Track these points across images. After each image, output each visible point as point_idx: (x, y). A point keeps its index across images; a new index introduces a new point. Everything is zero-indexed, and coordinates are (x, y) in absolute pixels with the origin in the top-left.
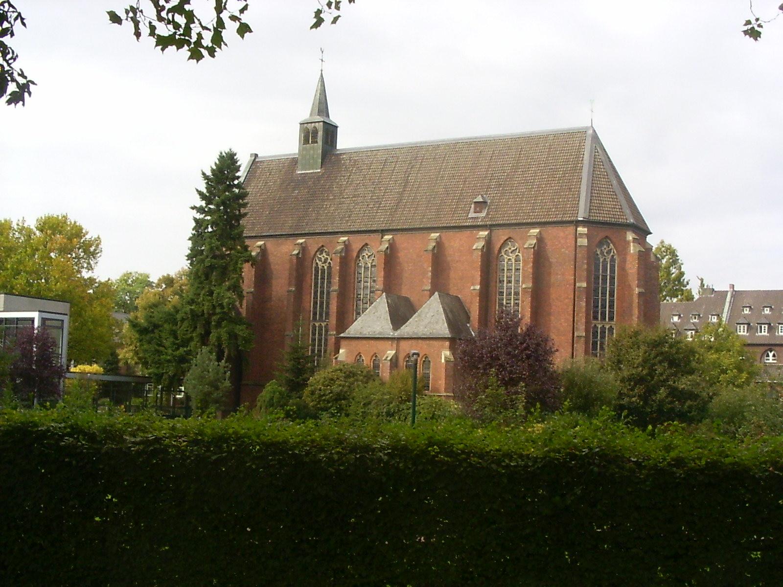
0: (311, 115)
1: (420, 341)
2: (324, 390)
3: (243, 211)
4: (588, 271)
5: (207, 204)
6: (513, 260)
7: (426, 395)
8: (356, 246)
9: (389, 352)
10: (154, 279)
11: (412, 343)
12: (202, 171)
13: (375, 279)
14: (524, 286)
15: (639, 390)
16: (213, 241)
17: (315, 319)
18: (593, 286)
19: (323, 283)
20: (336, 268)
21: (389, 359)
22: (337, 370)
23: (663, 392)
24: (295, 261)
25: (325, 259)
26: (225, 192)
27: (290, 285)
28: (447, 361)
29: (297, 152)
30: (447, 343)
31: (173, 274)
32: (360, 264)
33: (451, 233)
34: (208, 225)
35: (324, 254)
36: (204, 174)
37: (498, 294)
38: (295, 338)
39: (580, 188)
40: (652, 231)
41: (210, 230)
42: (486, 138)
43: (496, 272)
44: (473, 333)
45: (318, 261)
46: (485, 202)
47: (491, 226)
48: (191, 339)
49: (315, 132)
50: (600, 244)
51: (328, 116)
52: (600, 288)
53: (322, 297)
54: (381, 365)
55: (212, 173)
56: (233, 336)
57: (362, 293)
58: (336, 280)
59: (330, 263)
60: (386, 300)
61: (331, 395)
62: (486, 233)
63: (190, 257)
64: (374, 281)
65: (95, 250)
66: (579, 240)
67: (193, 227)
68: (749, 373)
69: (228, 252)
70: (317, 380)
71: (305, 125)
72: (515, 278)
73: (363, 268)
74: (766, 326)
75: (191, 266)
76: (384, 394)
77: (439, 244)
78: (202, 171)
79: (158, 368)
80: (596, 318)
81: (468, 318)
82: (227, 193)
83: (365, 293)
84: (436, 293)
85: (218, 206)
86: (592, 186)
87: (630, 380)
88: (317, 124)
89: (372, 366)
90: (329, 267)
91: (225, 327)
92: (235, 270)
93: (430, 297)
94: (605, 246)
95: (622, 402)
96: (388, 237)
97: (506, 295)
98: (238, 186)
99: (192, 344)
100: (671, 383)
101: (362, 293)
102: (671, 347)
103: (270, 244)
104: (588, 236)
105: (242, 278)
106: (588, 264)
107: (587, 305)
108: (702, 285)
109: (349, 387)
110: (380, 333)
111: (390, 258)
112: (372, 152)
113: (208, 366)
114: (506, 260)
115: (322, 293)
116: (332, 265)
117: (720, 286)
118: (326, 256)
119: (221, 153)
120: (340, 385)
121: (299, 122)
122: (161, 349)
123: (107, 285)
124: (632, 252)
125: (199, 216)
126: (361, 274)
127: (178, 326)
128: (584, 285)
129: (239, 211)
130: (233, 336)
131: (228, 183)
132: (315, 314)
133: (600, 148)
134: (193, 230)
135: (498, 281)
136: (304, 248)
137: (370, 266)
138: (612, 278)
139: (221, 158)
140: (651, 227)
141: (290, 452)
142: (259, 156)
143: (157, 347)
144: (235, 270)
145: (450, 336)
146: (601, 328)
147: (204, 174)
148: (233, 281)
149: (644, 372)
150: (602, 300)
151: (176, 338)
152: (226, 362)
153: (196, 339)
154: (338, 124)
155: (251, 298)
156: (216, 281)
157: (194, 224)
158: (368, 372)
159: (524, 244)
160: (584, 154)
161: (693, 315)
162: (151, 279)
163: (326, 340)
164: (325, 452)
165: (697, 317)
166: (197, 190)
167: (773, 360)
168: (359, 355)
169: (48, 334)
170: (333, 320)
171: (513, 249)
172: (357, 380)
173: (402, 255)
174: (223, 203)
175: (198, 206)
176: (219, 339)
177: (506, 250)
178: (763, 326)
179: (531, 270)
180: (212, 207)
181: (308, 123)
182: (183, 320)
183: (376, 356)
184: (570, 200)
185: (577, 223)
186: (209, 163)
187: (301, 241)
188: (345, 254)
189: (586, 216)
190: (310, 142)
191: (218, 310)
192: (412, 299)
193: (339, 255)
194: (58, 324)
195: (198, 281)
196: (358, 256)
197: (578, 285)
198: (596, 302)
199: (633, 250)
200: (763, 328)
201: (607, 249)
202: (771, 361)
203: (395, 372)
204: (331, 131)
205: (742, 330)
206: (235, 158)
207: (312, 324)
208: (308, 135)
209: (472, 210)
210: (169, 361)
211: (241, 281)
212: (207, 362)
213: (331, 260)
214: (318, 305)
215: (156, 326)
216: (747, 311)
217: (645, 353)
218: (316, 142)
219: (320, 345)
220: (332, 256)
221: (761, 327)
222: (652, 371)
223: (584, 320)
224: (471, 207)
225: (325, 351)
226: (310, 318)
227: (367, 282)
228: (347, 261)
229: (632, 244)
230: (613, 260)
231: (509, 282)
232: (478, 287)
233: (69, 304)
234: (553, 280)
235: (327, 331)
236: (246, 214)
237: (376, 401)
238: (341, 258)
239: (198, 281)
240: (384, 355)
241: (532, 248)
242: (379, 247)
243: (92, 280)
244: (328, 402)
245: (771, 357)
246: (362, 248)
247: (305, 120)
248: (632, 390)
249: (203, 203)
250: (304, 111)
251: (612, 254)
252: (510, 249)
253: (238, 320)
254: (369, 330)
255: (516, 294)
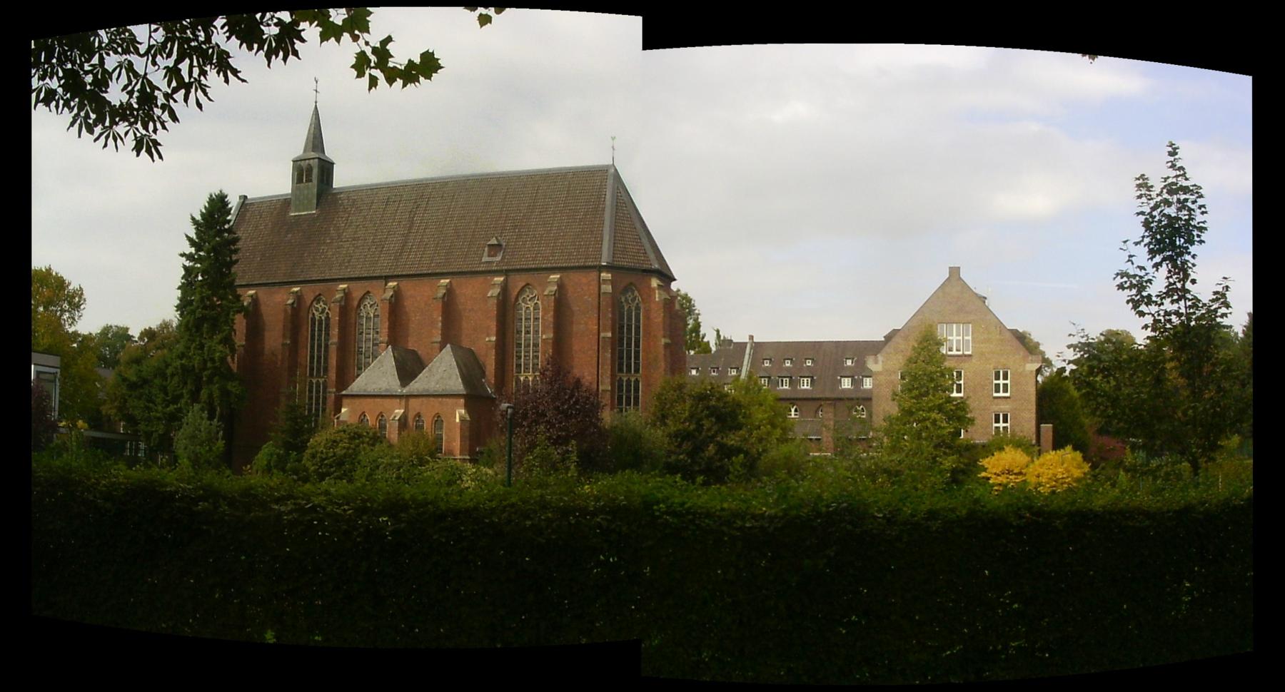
0: (305, 151)
1: (432, 399)
2: (327, 453)
3: (234, 257)
4: (613, 320)
5: (197, 251)
6: (532, 309)
7: (440, 459)
8: (357, 294)
9: (397, 411)
10: (135, 332)
12: (191, 216)
13: (379, 330)
14: (544, 337)
15: (687, 446)
16: (204, 290)
17: (311, 375)
18: (617, 335)
19: (320, 336)
20: (335, 319)
21: (397, 418)
22: (339, 431)
23: (712, 449)
24: (290, 311)
25: (322, 310)
26: (215, 237)
27: (284, 336)
28: (462, 420)
29: (290, 192)
30: (462, 401)
31: (154, 326)
32: (362, 314)
33: (462, 280)
34: (198, 273)
35: (321, 303)
36: (193, 219)
37: (515, 346)
38: (291, 396)
39: (602, 230)
40: (676, 277)
41: (200, 278)
42: (499, 174)
43: (514, 323)
44: (489, 389)
45: (314, 312)
46: (499, 245)
47: (507, 271)
48: (181, 396)
49: (310, 169)
50: (626, 290)
51: (323, 151)
52: (625, 339)
53: (319, 351)
54: (388, 425)
55: (201, 216)
56: (225, 393)
57: (364, 346)
58: (335, 331)
59: (327, 313)
60: (392, 354)
61: (335, 458)
62: (502, 279)
63: (179, 308)
64: (377, 333)
65: (79, 301)
66: (603, 287)
67: (181, 276)
68: (782, 429)
69: (219, 302)
70: (318, 441)
71: (299, 162)
72: (534, 328)
73: (365, 319)
74: (788, 379)
75: (181, 317)
76: (393, 457)
77: (450, 291)
78: (191, 216)
79: (147, 425)
80: (621, 370)
81: (483, 374)
82: (218, 239)
83: (367, 346)
84: (448, 346)
85: (208, 252)
86: (615, 229)
87: (676, 436)
88: (312, 161)
89: (378, 426)
90: (328, 318)
91: (217, 383)
92: (226, 322)
93: (441, 351)
95: (669, 460)
96: (392, 284)
97: (525, 347)
98: (230, 231)
99: (183, 401)
100: (719, 439)
101: (364, 346)
102: (718, 400)
103: (263, 293)
104: (613, 282)
105: (235, 331)
106: (613, 313)
107: (612, 357)
108: (718, 336)
109: (354, 449)
110: (387, 390)
111: (396, 308)
112: (373, 190)
113: (199, 425)
114: (524, 309)
115: (319, 346)
116: (330, 316)
117: (739, 337)
118: (323, 306)
119: (211, 196)
120: (344, 448)
121: (292, 159)
122: (151, 405)
123: (87, 338)
124: (657, 299)
125: (188, 264)
126: (362, 325)
127: (169, 382)
128: (609, 335)
129: (231, 257)
130: (225, 393)
131: (218, 228)
132: (312, 369)
133: (623, 188)
134: (182, 278)
135: (515, 331)
136: (299, 297)
137: (372, 315)
138: (638, 328)
139: (211, 200)
140: (675, 271)
141: (487, 521)
142: (248, 197)
143: (146, 404)
144: (226, 322)
145: (465, 393)
147: (193, 219)
148: (224, 334)
149: (692, 427)
150: (627, 351)
151: (166, 394)
152: (218, 421)
153: (186, 396)
154: (335, 162)
155: (243, 352)
156: (207, 333)
157: (183, 273)
158: (375, 433)
159: (543, 291)
160: (605, 195)
161: (712, 368)
162: (130, 333)
163: (325, 398)
164: (531, 519)
165: (716, 370)
166: (187, 236)
167: (795, 415)
168: (363, 414)
169: (42, 387)
170: (333, 375)
171: (531, 296)
172: (363, 443)
173: (408, 304)
174: (214, 249)
175: (187, 253)
176: (210, 396)
177: (524, 298)
178: (784, 379)
179: (551, 320)
180: (202, 253)
181: (301, 160)
182: (173, 375)
183: (382, 416)
184: (593, 243)
185: (601, 269)
186: (198, 206)
187: (296, 289)
188: (345, 303)
189: (610, 260)
191: (209, 365)
192: (420, 352)
193: (338, 304)
194: (51, 377)
195: (188, 333)
196: (359, 306)
197: (602, 335)
198: (621, 352)
199: (659, 298)
200: (784, 382)
201: (632, 296)
202: (793, 416)
203: (404, 434)
204: (326, 168)
205: (805, 384)
206: (226, 200)
207: (308, 380)
208: (301, 172)
209: (486, 254)
210: (159, 419)
211: (233, 333)
212: (199, 421)
213: (329, 309)
214: (315, 360)
215: (145, 382)
216: (767, 364)
217: (692, 407)
218: (311, 181)
219: (317, 404)
220: (330, 305)
221: (782, 381)
222: (700, 427)
223: (609, 372)
224: (484, 250)
225: (324, 410)
226: (306, 374)
227: (370, 334)
228: (348, 310)
229: (657, 292)
230: (638, 308)
231: (528, 332)
232: (494, 339)
233: (59, 358)
234: (575, 328)
235: (325, 388)
236: (237, 261)
237: (384, 465)
238: (341, 307)
239: (188, 333)
240: (392, 414)
241: (551, 295)
242: (382, 295)
243: (76, 334)
244: (331, 467)
245: (793, 413)
246: (364, 295)
247: (298, 157)
248: (679, 446)
249: (193, 250)
250: (297, 147)
251: (637, 301)
252: (528, 296)
253: (227, 375)
254: (374, 386)
255: (536, 345)
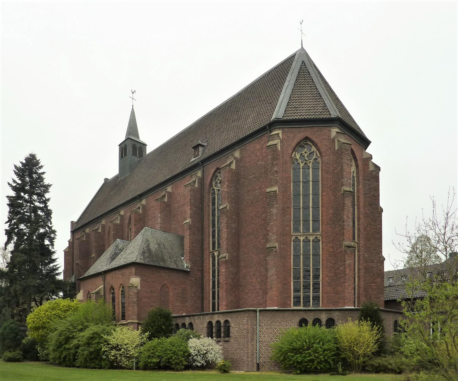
50: (300, 145)
94: (306, 150)
146: (313, 240)
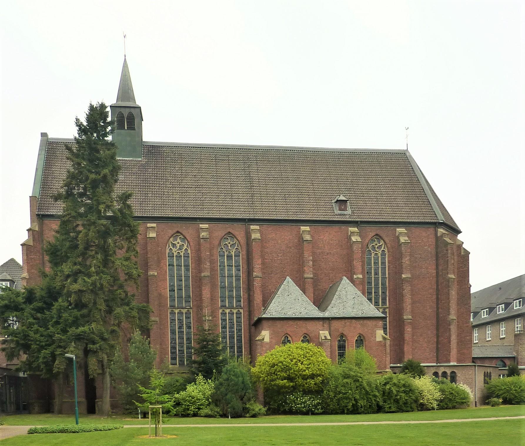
1: (354, 321)
11: (345, 323)
190: (126, 128)
